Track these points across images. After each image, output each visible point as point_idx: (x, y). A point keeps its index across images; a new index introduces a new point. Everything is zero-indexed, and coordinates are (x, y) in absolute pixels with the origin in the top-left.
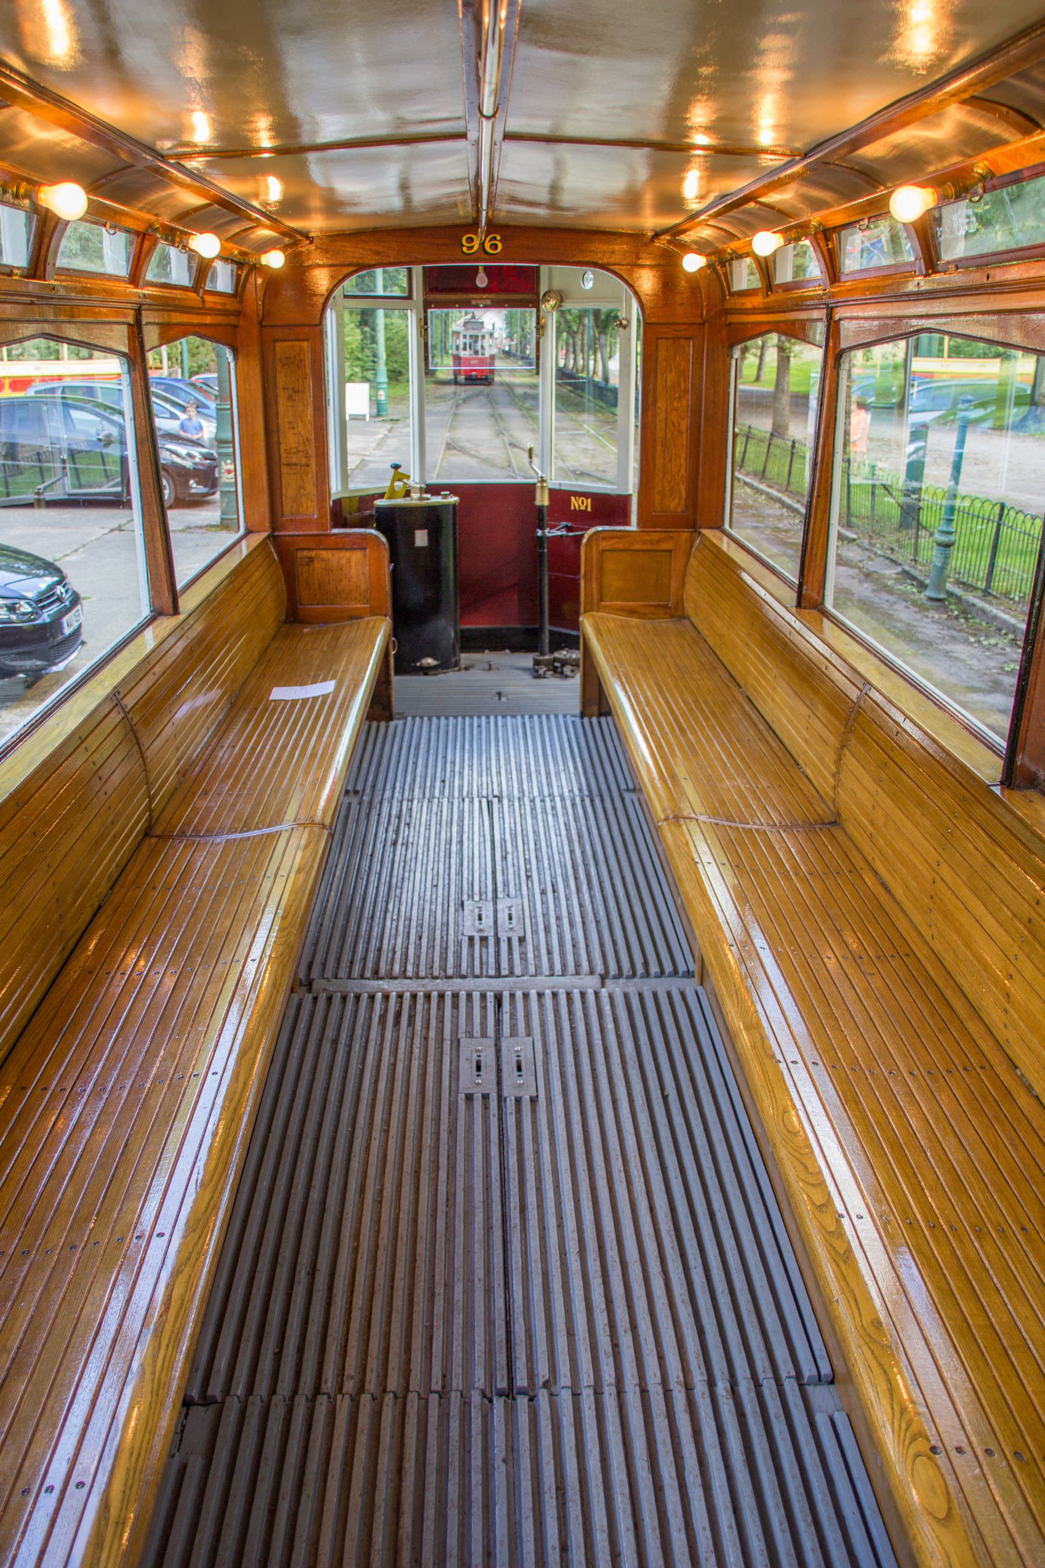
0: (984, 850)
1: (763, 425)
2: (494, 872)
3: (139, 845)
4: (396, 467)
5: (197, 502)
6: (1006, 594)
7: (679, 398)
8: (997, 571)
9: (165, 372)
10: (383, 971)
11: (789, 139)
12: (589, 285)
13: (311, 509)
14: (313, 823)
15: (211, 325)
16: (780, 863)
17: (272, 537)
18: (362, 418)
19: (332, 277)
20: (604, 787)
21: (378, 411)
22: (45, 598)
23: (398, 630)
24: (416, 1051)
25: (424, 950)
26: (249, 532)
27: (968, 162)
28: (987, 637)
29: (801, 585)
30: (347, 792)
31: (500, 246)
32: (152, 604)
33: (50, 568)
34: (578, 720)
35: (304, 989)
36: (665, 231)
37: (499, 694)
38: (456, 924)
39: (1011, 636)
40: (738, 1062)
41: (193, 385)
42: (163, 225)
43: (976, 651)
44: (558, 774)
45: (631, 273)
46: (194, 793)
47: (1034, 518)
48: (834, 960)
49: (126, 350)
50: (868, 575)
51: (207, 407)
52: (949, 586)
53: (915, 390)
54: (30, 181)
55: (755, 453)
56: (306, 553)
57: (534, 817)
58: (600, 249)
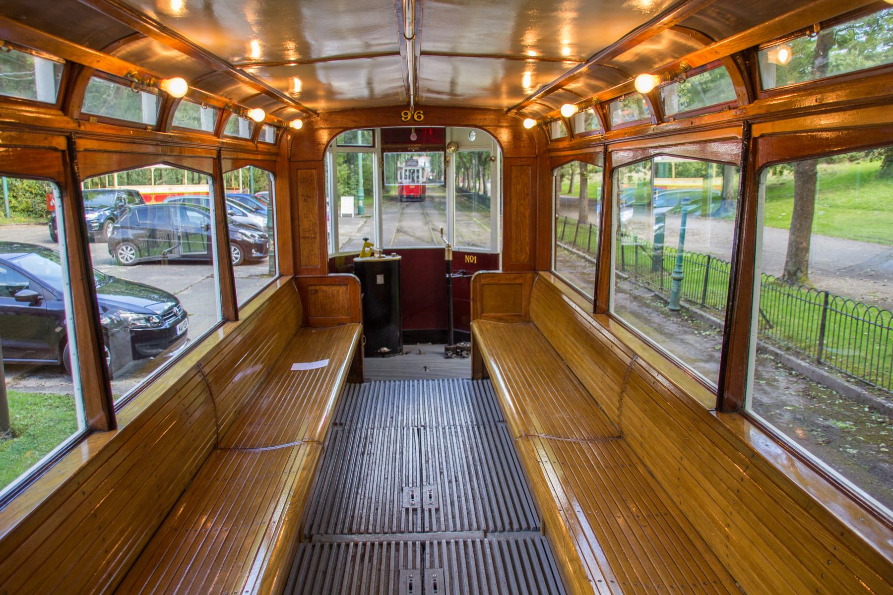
0: (708, 449)
1: (574, 216)
2: (421, 470)
3: (210, 454)
4: (366, 240)
5: (257, 262)
6: (714, 306)
7: (524, 199)
8: (708, 293)
9: (241, 191)
10: (354, 529)
11: (579, 53)
12: (473, 139)
13: (317, 262)
14: (313, 441)
15: (261, 160)
16: (588, 461)
17: (295, 279)
18: (349, 216)
19: (330, 134)
20: (485, 420)
21: (359, 211)
22: (167, 314)
23: (366, 331)
24: (373, 577)
25: (379, 516)
26: (281, 276)
27: (677, 61)
28: (705, 331)
29: (595, 300)
30: (335, 424)
31: (423, 117)
32: (223, 315)
33: (171, 297)
34: (470, 382)
35: (307, 540)
36: (513, 108)
37: (425, 368)
38: (398, 501)
39: (718, 330)
40: (566, 582)
41: (256, 197)
42: (234, 105)
43: (700, 339)
44: (459, 413)
45: (495, 130)
46: (244, 424)
47: (727, 263)
48: (622, 519)
49: (211, 172)
50: (635, 298)
51: (262, 209)
52: (681, 303)
53: (657, 195)
54: (156, 78)
55: (570, 231)
56: (313, 288)
57: (445, 438)
58: (479, 118)
